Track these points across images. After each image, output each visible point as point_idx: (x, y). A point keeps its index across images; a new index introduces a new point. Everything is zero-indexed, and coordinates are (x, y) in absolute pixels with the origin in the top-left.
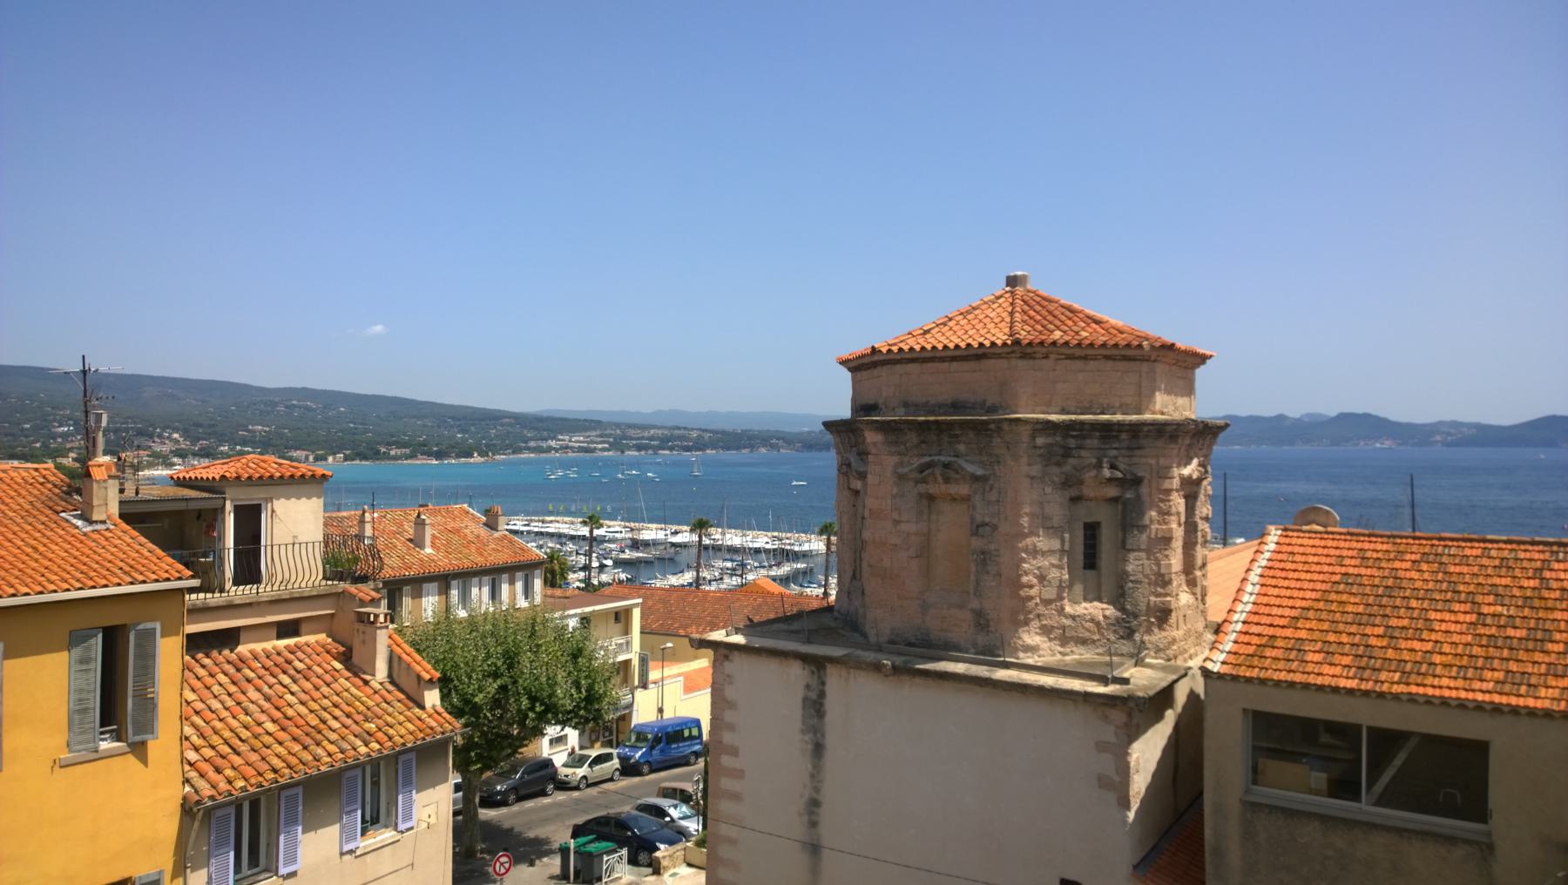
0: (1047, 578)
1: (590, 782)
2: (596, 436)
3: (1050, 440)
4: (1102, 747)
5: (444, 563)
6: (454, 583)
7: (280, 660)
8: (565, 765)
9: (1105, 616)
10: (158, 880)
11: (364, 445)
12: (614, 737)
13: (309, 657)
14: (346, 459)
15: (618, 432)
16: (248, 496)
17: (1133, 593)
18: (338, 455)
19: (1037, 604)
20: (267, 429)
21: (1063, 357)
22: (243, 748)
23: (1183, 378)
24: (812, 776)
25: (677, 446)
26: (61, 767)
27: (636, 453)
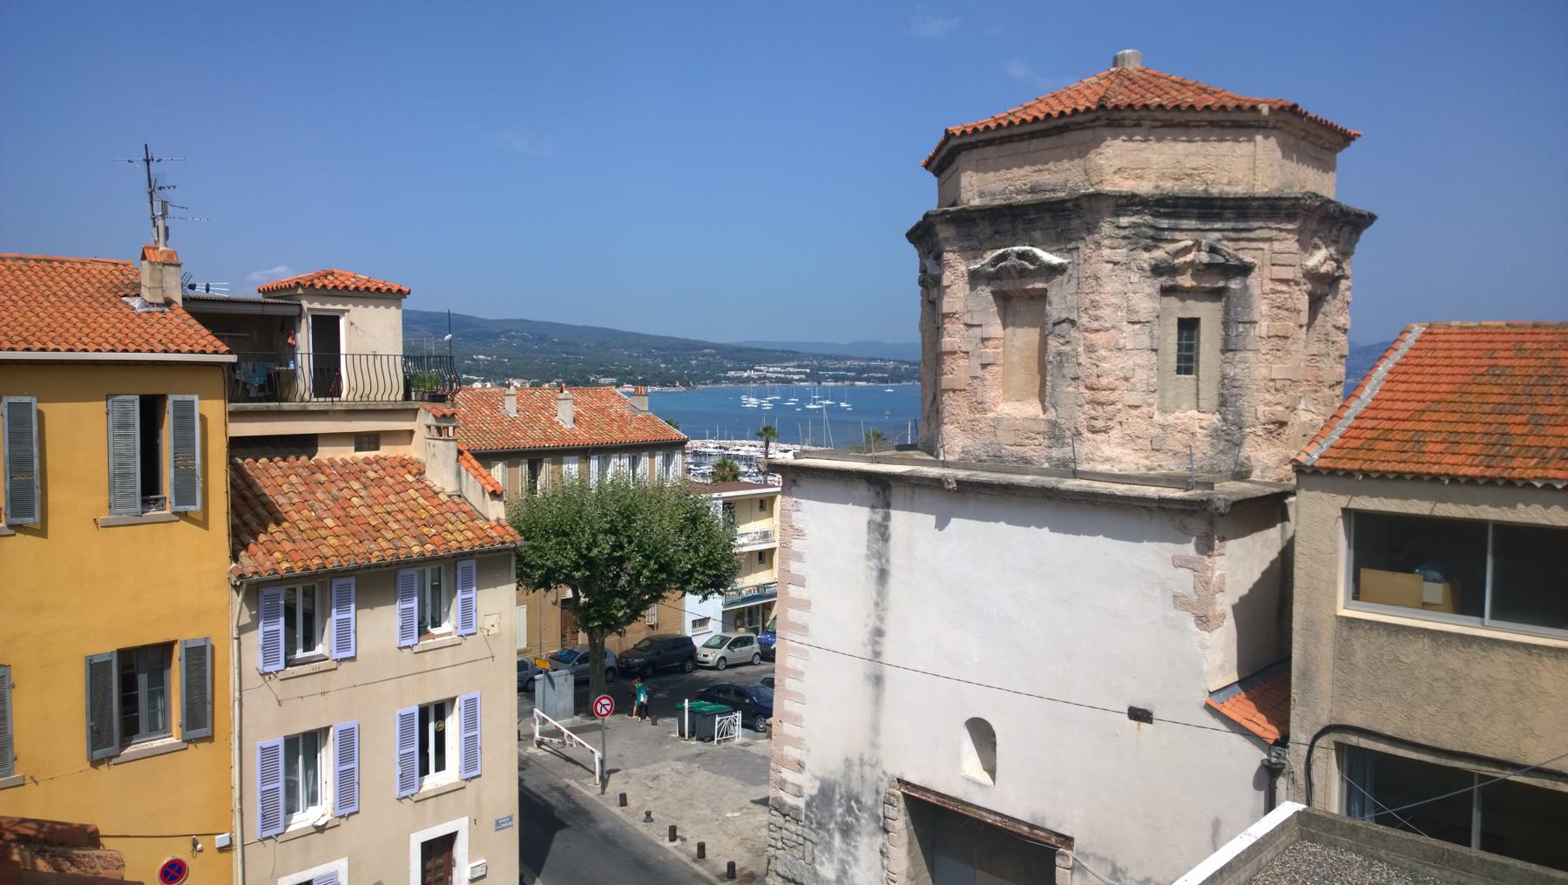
1: (728, 663)
2: (793, 367)
5: (584, 437)
8: (706, 646)
9: (1201, 427)
12: (760, 626)
13: (384, 469)
15: (815, 363)
17: (1236, 401)
21: (1158, 124)
23: (1317, 159)
24: (877, 604)
27: (833, 384)
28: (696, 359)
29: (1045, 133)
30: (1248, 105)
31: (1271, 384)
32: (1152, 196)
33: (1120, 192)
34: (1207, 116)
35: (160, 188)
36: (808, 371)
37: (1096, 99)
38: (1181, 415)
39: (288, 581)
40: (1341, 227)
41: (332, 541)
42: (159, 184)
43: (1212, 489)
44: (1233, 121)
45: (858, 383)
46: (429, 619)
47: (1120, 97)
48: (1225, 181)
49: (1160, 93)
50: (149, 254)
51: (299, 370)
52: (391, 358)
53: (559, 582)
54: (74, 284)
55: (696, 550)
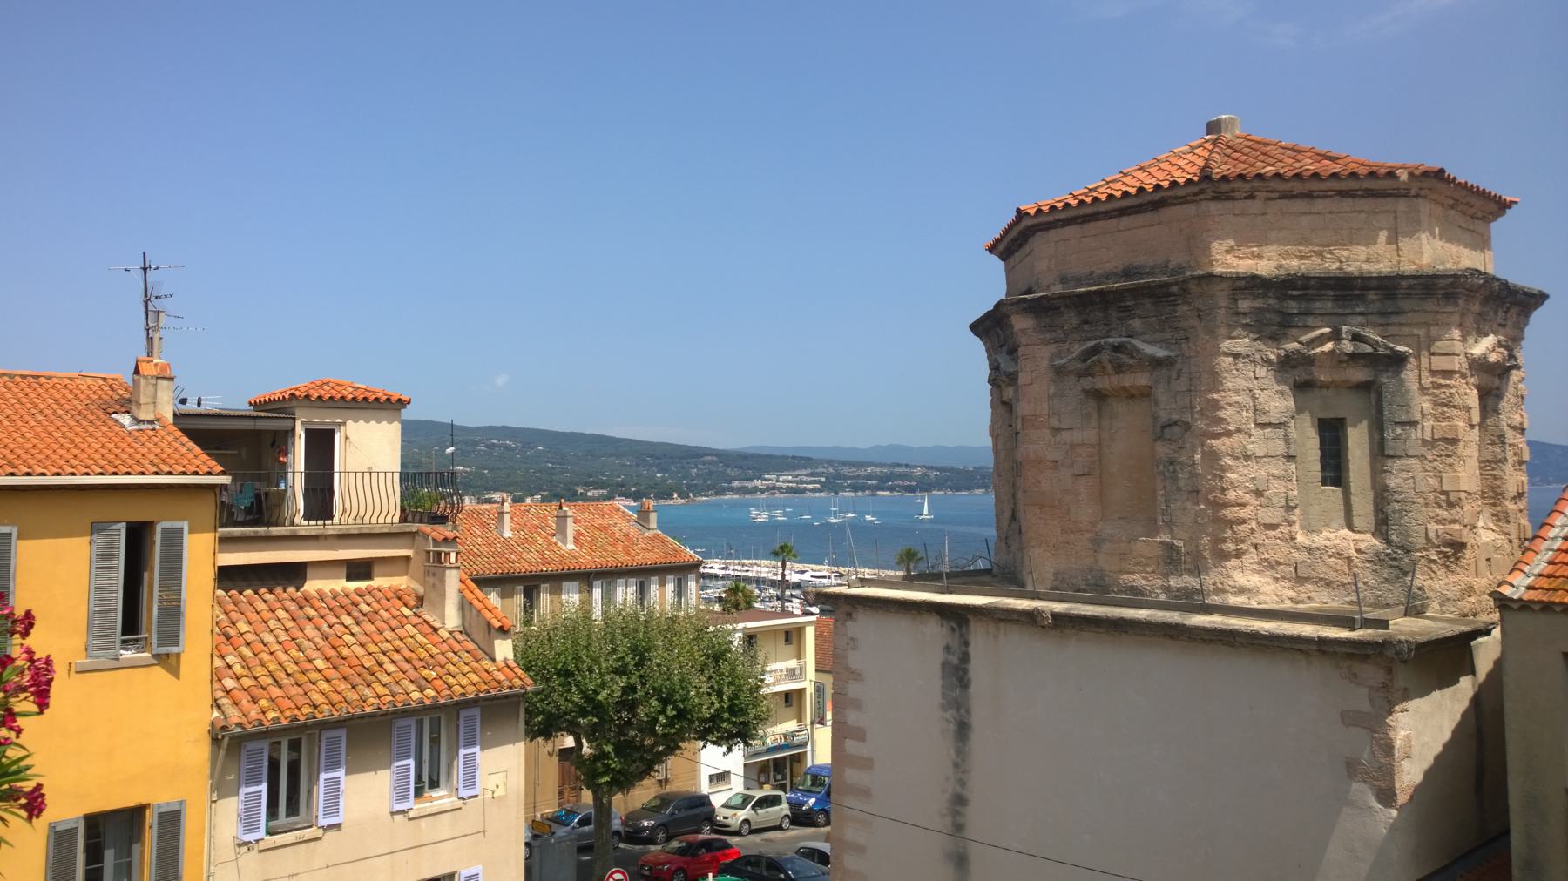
0: (1266, 494)
1: (753, 827)
3: (1259, 304)
4: (1350, 719)
5: (586, 560)
6: (597, 583)
7: (346, 601)
8: (726, 806)
9: (1358, 551)
10: (179, 812)
11: (562, 485)
12: (788, 782)
13: (378, 602)
14: (543, 501)
15: (831, 470)
16: (321, 419)
17: (1401, 518)
18: (535, 497)
19: (1252, 531)
20: (468, 470)
21: (1276, 195)
22: (285, 681)
23: (1469, 230)
24: (956, 765)
25: (898, 486)
26: (77, 672)
27: (852, 494)
28: (696, 466)
29: (1137, 209)
30: (1383, 171)
31: (1443, 497)
32: (1276, 277)
33: (1237, 273)
34: (1334, 185)
35: (156, 298)
36: (823, 479)
37: (1195, 170)
38: (1331, 536)
39: (271, 735)
40: (1509, 309)
41: (324, 686)
42: (155, 293)
43: (1387, 627)
44: (1366, 190)
45: (880, 493)
46: (426, 778)
47: (1225, 167)
48: (1363, 257)
49: (1271, 161)
50: (143, 367)
51: (290, 490)
52: (389, 475)
53: (562, 730)
54: (62, 401)
55: (720, 694)
